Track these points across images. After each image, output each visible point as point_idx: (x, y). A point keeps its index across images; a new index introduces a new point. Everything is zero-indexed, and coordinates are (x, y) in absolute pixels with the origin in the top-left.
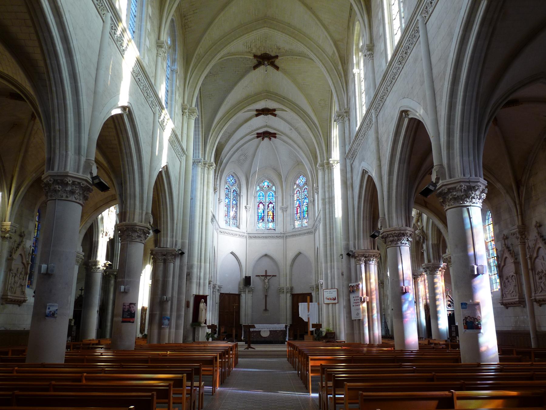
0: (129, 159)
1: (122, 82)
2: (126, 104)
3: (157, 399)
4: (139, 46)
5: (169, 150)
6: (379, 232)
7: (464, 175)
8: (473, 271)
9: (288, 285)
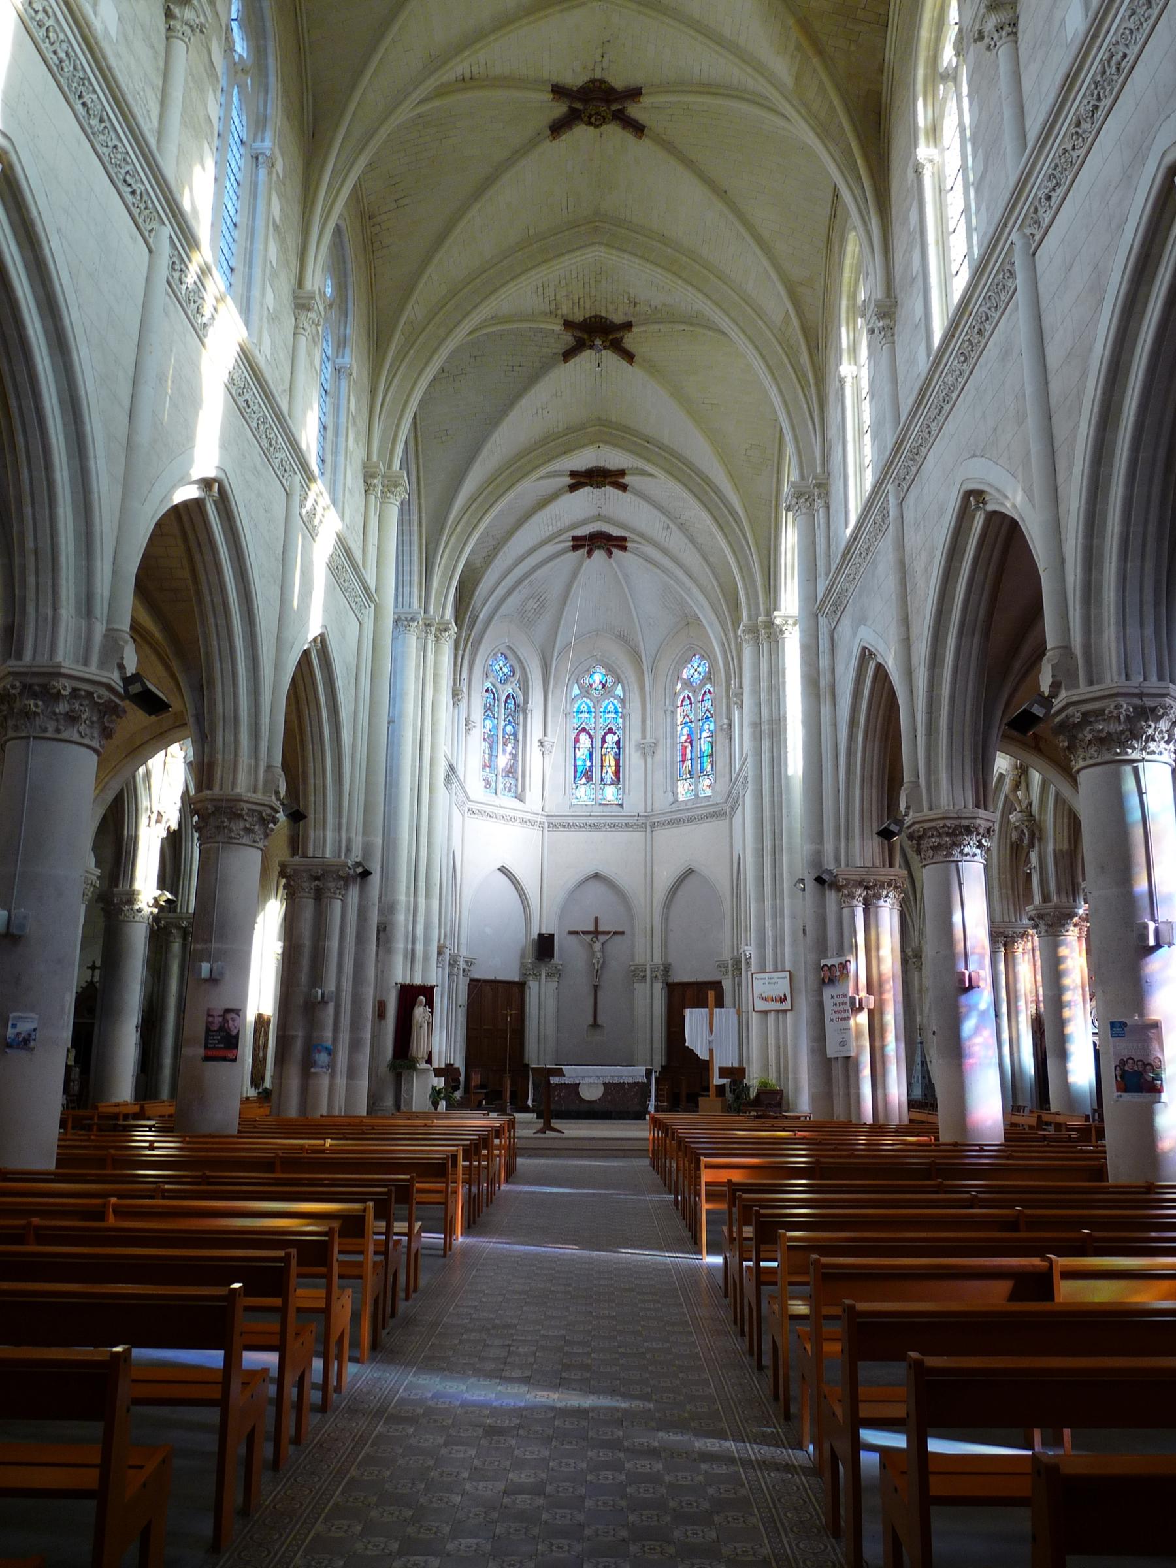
0: (225, 644)
1: (201, 413)
2: (211, 473)
3: (299, 1264)
4: (246, 310)
5: (329, 592)
6: (900, 823)
7: (1127, 677)
8: (1146, 938)
9: (657, 959)
